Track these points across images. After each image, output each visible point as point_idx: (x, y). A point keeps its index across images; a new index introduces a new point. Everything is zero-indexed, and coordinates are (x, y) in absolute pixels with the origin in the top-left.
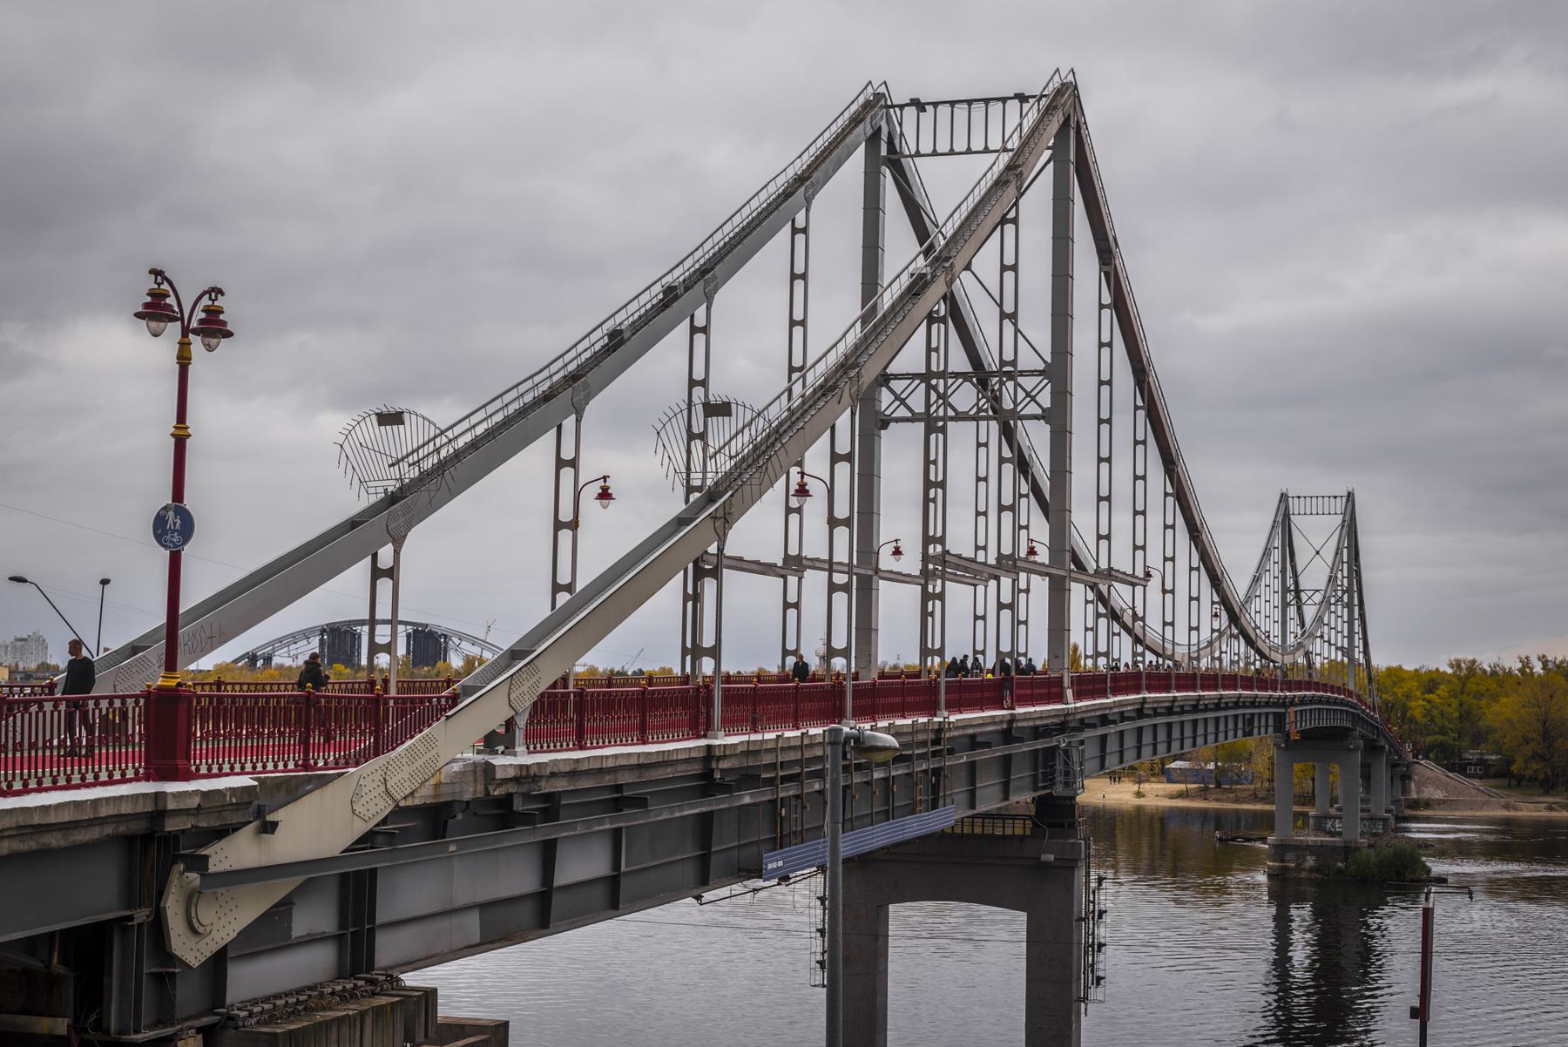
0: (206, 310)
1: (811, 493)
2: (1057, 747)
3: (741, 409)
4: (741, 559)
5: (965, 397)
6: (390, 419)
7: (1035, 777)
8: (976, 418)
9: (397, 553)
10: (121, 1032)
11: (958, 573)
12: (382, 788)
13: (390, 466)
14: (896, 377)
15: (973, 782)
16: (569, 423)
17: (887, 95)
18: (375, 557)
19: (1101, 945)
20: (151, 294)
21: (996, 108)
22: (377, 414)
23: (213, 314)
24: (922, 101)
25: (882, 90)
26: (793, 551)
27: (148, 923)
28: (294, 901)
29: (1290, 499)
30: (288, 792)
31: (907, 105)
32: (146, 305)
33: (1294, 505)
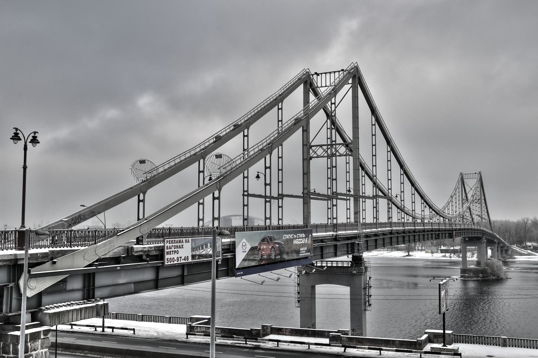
0: (33, 137)
1: (260, 177)
2: (354, 243)
3: (224, 156)
4: (341, 193)
5: (342, 150)
6: (142, 162)
7: (348, 251)
8: (346, 155)
9: (144, 196)
10: (7, 312)
11: (319, 197)
12: (95, 253)
13: (218, 169)
14: (314, 146)
15: (322, 251)
16: (268, 157)
17: (309, 72)
18: (213, 194)
19: (370, 296)
20: (14, 133)
21: (328, 75)
22: (215, 155)
23: (35, 138)
24: (318, 73)
25: (308, 71)
26: (280, 193)
27: (14, 286)
28: (68, 281)
29: (463, 175)
30: (62, 254)
31: (341, 71)
32: (13, 136)
33: (464, 177)
